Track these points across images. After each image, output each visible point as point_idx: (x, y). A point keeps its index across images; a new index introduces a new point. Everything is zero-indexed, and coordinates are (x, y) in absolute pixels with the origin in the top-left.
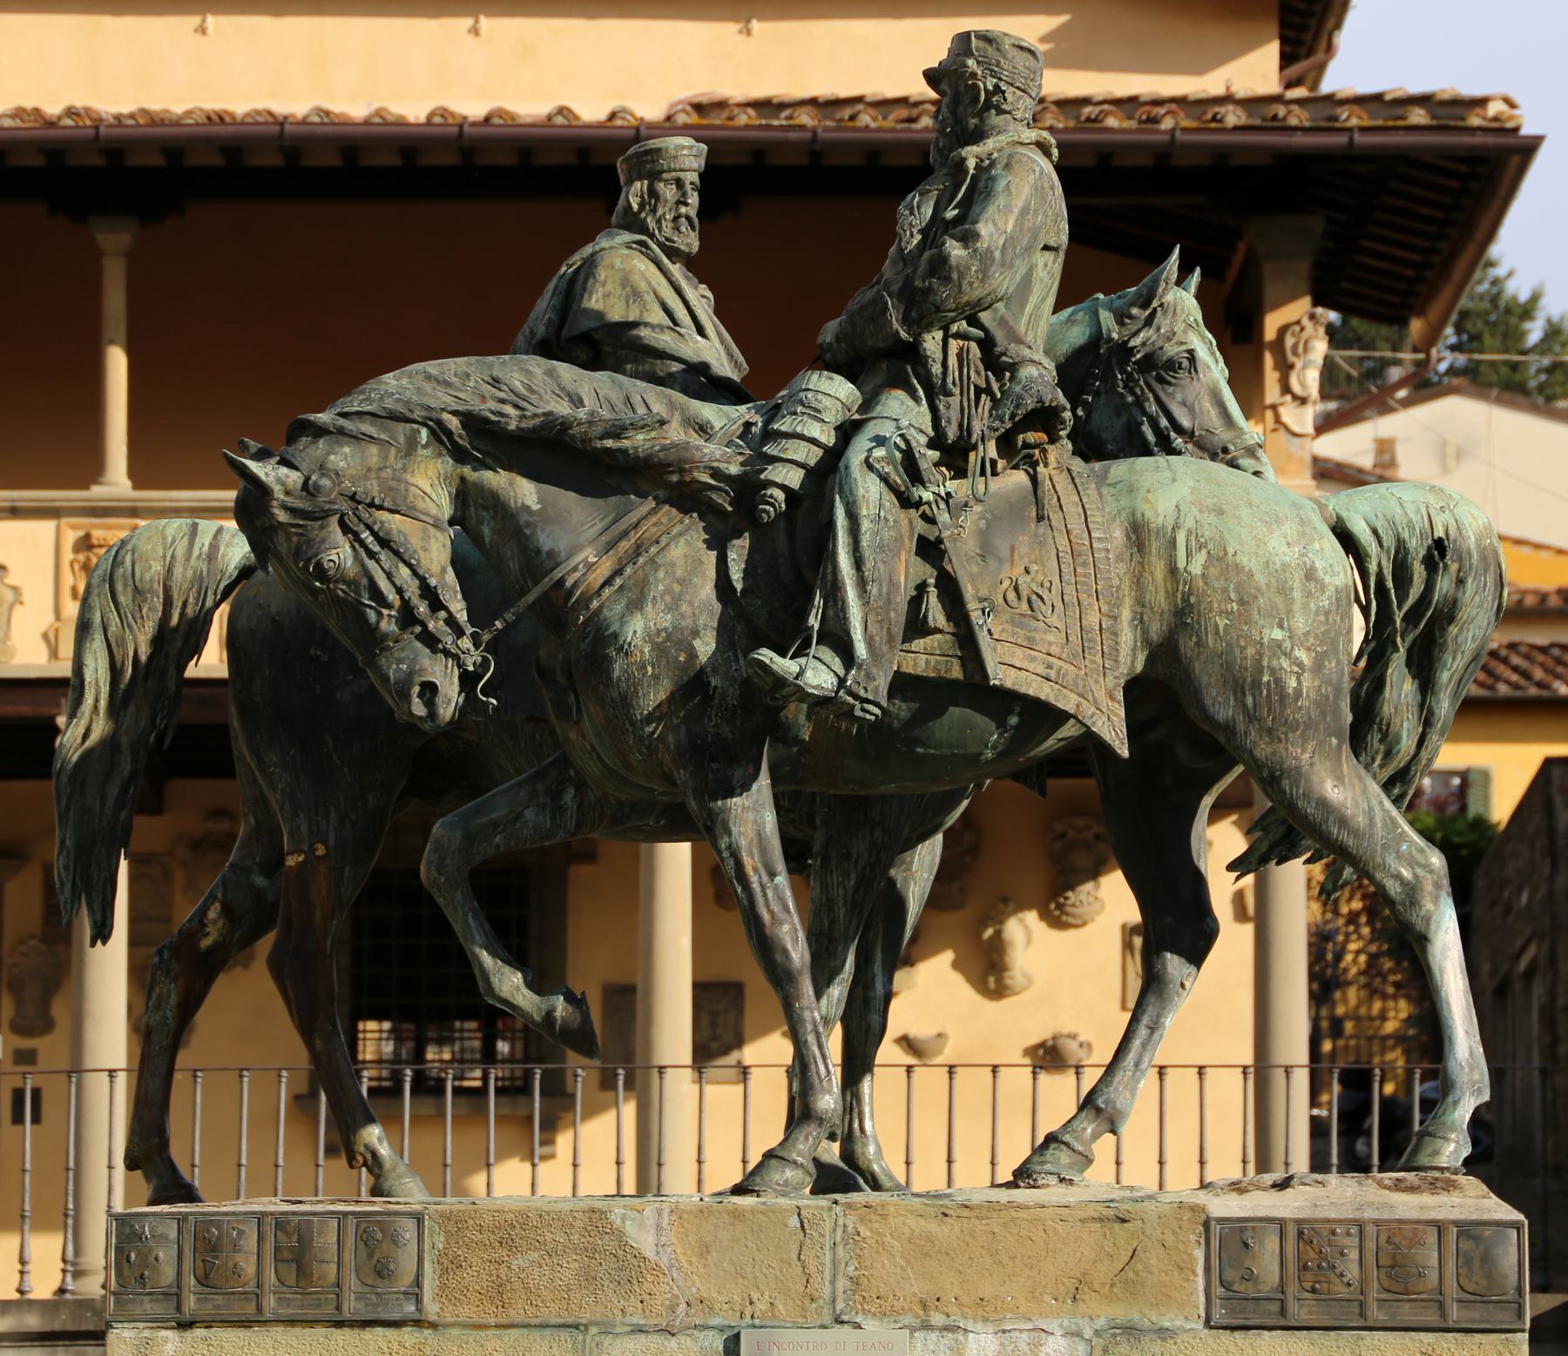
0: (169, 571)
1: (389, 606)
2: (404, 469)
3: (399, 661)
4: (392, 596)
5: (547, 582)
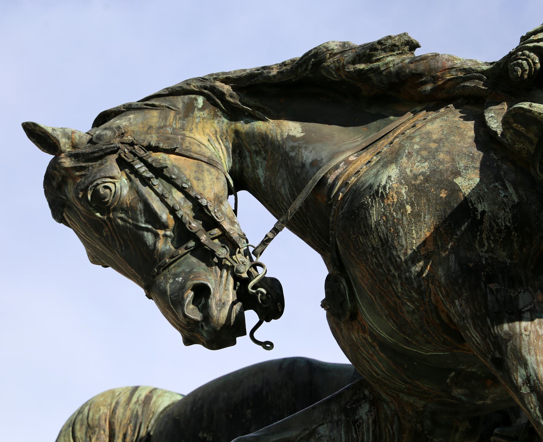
0: (114, 412)
1: (164, 226)
2: (183, 128)
3: (177, 275)
4: (165, 216)
5: (311, 184)
